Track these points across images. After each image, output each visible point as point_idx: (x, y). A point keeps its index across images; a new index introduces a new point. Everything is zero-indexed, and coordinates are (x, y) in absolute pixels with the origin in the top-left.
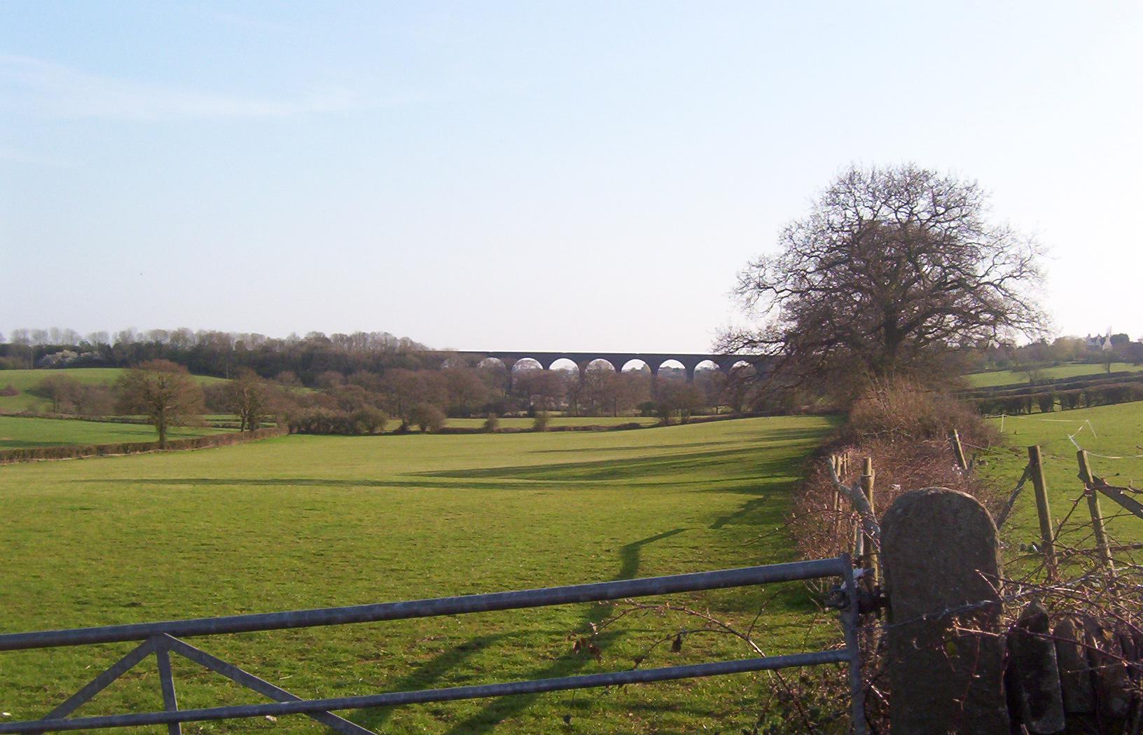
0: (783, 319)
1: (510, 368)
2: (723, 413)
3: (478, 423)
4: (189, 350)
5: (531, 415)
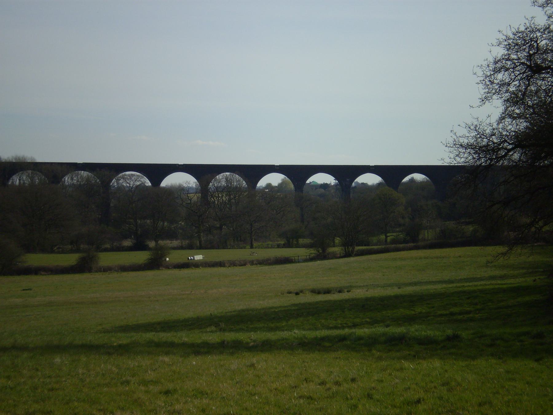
0: (506, 115)
1: (106, 184)
2: (394, 242)
3: (71, 259)
4: (265, 186)
5: (139, 246)
